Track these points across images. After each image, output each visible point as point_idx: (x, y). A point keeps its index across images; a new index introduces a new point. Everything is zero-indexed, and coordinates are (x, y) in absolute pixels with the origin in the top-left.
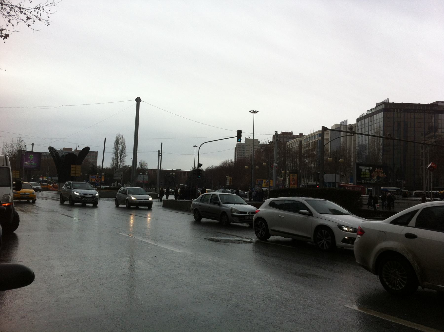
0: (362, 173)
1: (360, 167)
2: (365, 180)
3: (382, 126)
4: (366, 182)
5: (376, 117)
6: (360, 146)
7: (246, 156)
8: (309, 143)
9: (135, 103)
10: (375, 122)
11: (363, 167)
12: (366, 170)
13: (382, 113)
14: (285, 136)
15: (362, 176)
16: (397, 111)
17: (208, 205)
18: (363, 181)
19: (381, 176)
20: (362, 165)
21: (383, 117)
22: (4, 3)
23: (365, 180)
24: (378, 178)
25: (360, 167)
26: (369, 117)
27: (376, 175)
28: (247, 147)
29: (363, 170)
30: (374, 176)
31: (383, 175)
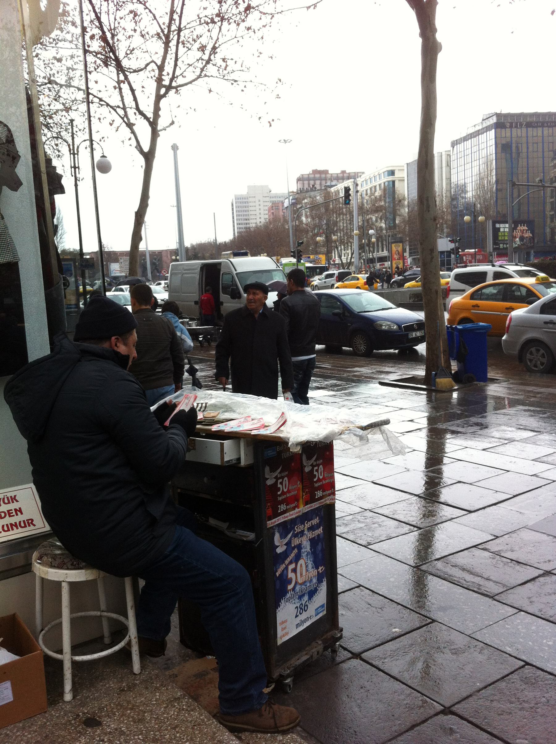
0: (500, 234)
1: (497, 226)
2: (504, 244)
3: (494, 152)
4: (505, 246)
5: (483, 137)
6: (457, 186)
7: (251, 225)
8: (375, 187)
9: (172, 152)
10: (482, 146)
11: (502, 225)
12: (504, 228)
13: (493, 130)
14: (317, 176)
15: (500, 238)
16: (516, 127)
17: (28, 631)
18: (501, 246)
19: (526, 235)
20: (500, 222)
21: (496, 138)
22: (49, 85)
23: (504, 244)
24: (522, 239)
25: (497, 226)
26: (471, 138)
27: (519, 234)
28: (250, 200)
29: (502, 230)
30: (516, 237)
31: (528, 235)
